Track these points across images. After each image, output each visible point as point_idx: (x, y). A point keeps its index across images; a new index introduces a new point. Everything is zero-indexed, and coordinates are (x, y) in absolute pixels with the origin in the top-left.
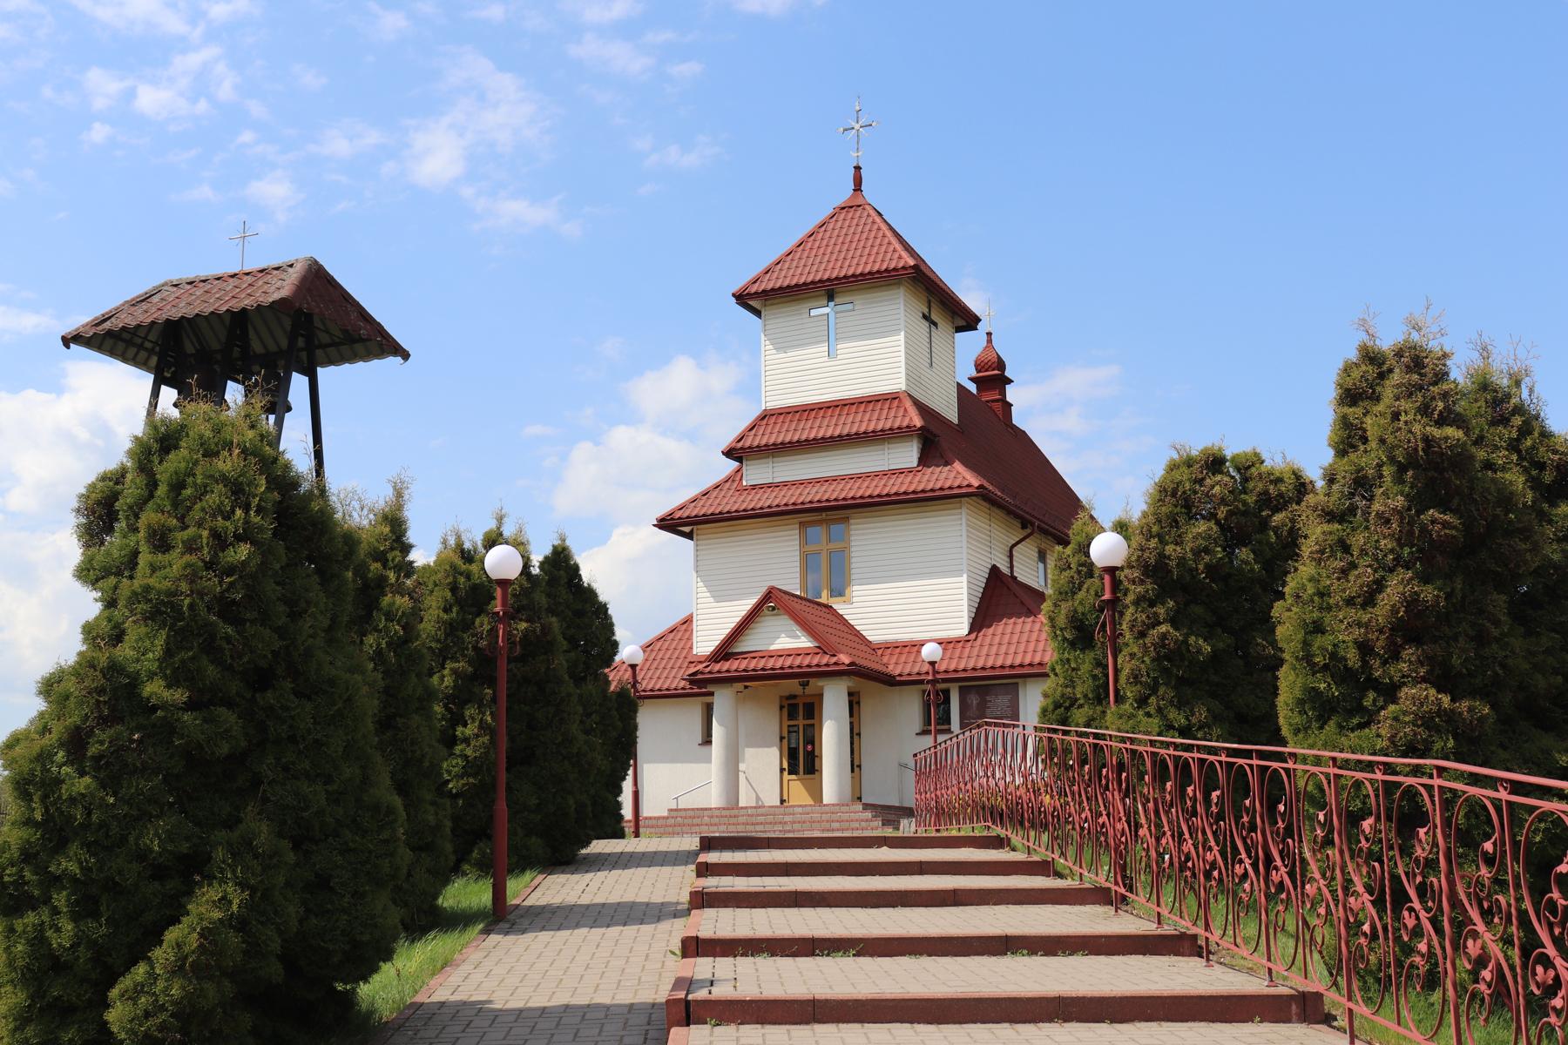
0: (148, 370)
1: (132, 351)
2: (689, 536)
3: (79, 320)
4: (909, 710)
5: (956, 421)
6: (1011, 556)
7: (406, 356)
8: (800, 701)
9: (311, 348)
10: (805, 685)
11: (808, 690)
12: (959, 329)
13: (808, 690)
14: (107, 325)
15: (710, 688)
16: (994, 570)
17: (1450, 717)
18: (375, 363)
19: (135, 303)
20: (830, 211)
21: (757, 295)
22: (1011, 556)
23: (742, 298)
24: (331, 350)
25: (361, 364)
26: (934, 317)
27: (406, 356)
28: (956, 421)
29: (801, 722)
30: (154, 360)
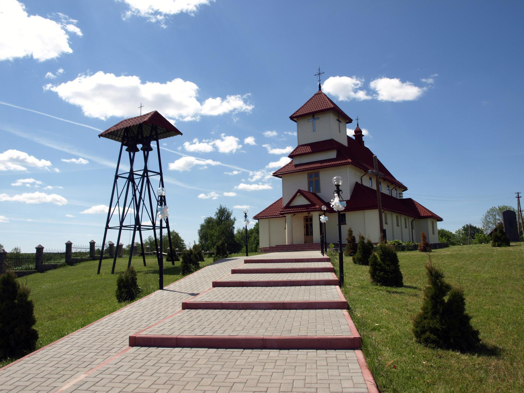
0: (119, 141)
1: (117, 138)
2: (281, 177)
3: (102, 131)
4: (190, 239)
5: (347, 146)
6: (361, 179)
7: (182, 134)
8: (309, 218)
9: (157, 134)
10: (309, 213)
11: (310, 215)
12: (347, 123)
13: (310, 215)
14: (110, 131)
15: (285, 215)
16: (357, 183)
17: (377, 258)
18: (175, 136)
19: (115, 126)
20: (313, 95)
21: (295, 117)
22: (361, 179)
23: (292, 118)
24: (161, 135)
25: (172, 137)
26: (340, 120)
27: (182, 134)
28: (347, 146)
29: (309, 223)
30: (120, 139)
